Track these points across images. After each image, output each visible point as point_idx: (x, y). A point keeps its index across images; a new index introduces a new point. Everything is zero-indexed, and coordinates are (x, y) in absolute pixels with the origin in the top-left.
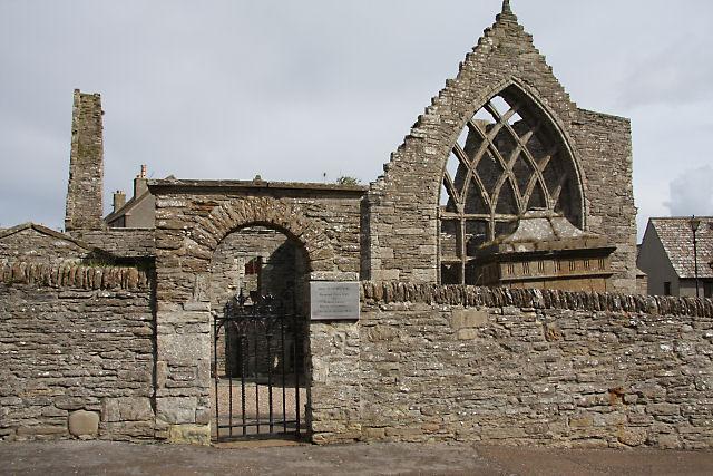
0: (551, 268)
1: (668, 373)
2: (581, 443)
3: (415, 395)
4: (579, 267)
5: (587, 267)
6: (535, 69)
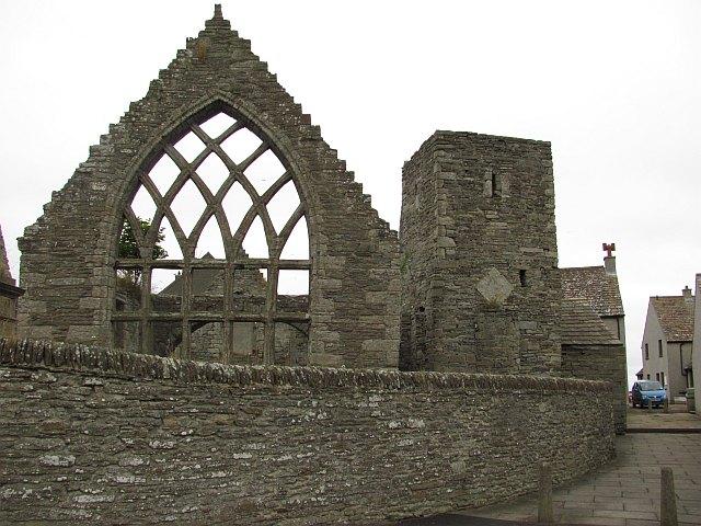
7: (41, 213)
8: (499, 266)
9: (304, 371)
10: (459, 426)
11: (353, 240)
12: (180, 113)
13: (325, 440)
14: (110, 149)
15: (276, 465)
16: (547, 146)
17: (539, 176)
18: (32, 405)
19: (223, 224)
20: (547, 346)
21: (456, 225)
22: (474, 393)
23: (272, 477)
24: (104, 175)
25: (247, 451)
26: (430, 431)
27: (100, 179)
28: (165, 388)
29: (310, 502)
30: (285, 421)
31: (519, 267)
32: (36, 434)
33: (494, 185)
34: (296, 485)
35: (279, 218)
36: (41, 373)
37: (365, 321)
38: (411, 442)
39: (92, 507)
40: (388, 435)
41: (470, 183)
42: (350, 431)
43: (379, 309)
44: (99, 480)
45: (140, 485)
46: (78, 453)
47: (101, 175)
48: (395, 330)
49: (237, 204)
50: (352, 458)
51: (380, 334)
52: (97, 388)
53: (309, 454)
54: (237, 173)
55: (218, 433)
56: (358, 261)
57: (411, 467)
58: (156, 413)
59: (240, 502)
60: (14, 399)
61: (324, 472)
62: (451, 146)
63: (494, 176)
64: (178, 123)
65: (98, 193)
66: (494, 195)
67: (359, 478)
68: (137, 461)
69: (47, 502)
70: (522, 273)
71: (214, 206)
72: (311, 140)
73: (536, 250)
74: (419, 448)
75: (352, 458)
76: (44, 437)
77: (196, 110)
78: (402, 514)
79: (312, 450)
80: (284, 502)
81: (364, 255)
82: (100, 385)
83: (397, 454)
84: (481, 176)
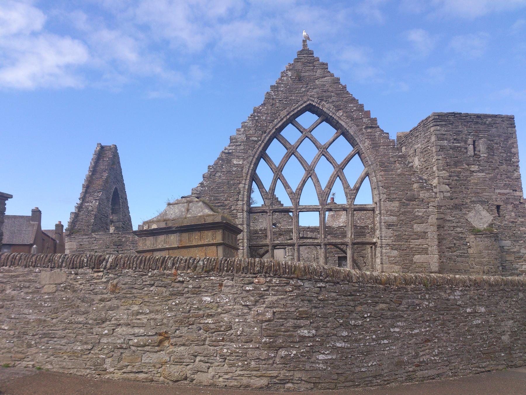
0: (173, 240)
1: (210, 321)
2: (131, 375)
3: (12, 333)
4: (195, 239)
5: (214, 238)
6: (331, 89)
7: (201, 180)
8: (482, 203)
9: (419, 276)
10: (503, 312)
11: (403, 190)
12: (286, 113)
13: (435, 320)
14: (243, 138)
15: (412, 336)
16: (511, 119)
17: (507, 139)
18: (292, 300)
19: (317, 183)
20: (520, 258)
21: (450, 176)
22: (509, 290)
23: (410, 344)
24: (240, 154)
25: (398, 327)
26: (488, 315)
27: (238, 157)
28: (355, 288)
29: (431, 360)
30: (413, 307)
31: (496, 203)
32: (295, 317)
33: (474, 148)
34: (423, 349)
35: (352, 179)
36: (295, 280)
37: (414, 243)
38: (480, 322)
39: (325, 362)
40: (467, 317)
41: (458, 147)
42: (447, 314)
43: (423, 235)
44: (328, 346)
45: (348, 348)
46: (317, 329)
47: (238, 154)
48: (434, 248)
49: (324, 171)
50: (450, 331)
51: (425, 251)
52: (322, 289)
53: (428, 329)
54: (324, 151)
55: (380, 317)
56: (408, 205)
57: (481, 338)
58: (351, 303)
59: (396, 360)
60: (282, 297)
61: (436, 341)
62: (443, 123)
63: (474, 142)
64: (285, 120)
65: (237, 166)
66: (475, 154)
67: (455, 345)
68: (345, 334)
69: (304, 359)
70: (498, 207)
71: (310, 172)
72: (371, 127)
73: (507, 191)
74: (483, 325)
75: (450, 331)
76: (299, 319)
77: (296, 111)
78: (479, 369)
79: (429, 326)
80: (418, 360)
81: (411, 200)
82: (324, 287)
83: (473, 330)
84: (466, 142)
